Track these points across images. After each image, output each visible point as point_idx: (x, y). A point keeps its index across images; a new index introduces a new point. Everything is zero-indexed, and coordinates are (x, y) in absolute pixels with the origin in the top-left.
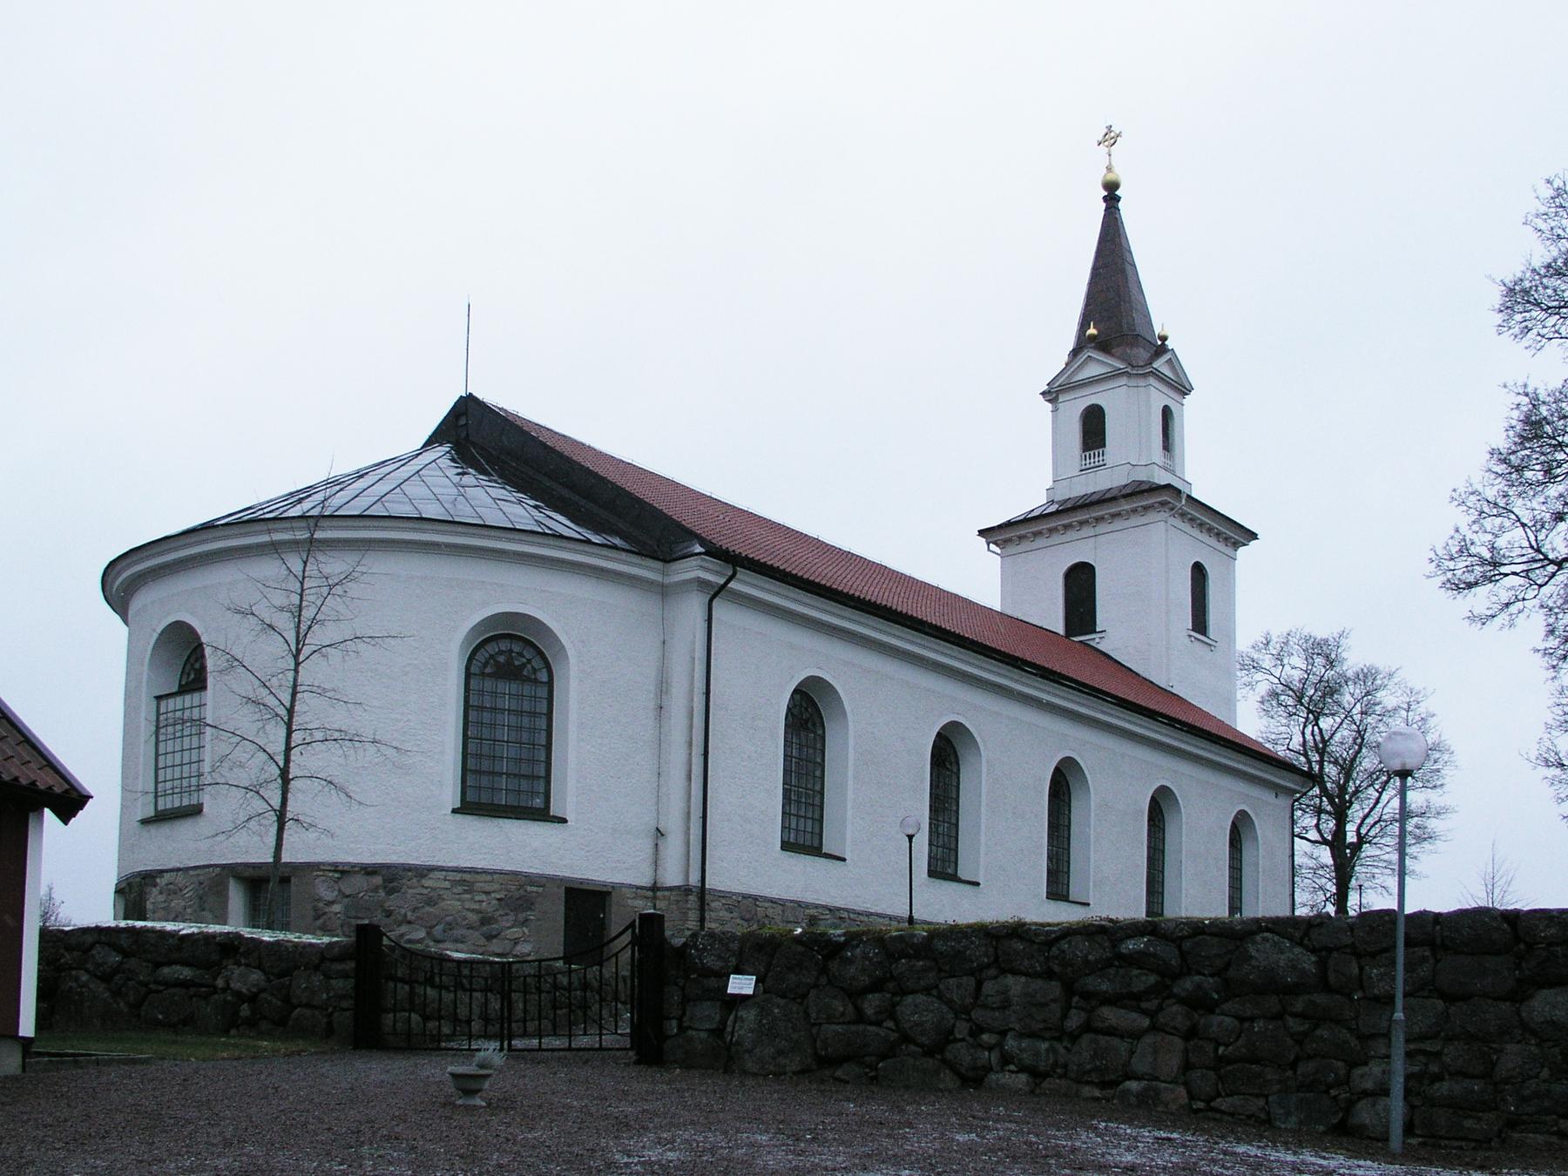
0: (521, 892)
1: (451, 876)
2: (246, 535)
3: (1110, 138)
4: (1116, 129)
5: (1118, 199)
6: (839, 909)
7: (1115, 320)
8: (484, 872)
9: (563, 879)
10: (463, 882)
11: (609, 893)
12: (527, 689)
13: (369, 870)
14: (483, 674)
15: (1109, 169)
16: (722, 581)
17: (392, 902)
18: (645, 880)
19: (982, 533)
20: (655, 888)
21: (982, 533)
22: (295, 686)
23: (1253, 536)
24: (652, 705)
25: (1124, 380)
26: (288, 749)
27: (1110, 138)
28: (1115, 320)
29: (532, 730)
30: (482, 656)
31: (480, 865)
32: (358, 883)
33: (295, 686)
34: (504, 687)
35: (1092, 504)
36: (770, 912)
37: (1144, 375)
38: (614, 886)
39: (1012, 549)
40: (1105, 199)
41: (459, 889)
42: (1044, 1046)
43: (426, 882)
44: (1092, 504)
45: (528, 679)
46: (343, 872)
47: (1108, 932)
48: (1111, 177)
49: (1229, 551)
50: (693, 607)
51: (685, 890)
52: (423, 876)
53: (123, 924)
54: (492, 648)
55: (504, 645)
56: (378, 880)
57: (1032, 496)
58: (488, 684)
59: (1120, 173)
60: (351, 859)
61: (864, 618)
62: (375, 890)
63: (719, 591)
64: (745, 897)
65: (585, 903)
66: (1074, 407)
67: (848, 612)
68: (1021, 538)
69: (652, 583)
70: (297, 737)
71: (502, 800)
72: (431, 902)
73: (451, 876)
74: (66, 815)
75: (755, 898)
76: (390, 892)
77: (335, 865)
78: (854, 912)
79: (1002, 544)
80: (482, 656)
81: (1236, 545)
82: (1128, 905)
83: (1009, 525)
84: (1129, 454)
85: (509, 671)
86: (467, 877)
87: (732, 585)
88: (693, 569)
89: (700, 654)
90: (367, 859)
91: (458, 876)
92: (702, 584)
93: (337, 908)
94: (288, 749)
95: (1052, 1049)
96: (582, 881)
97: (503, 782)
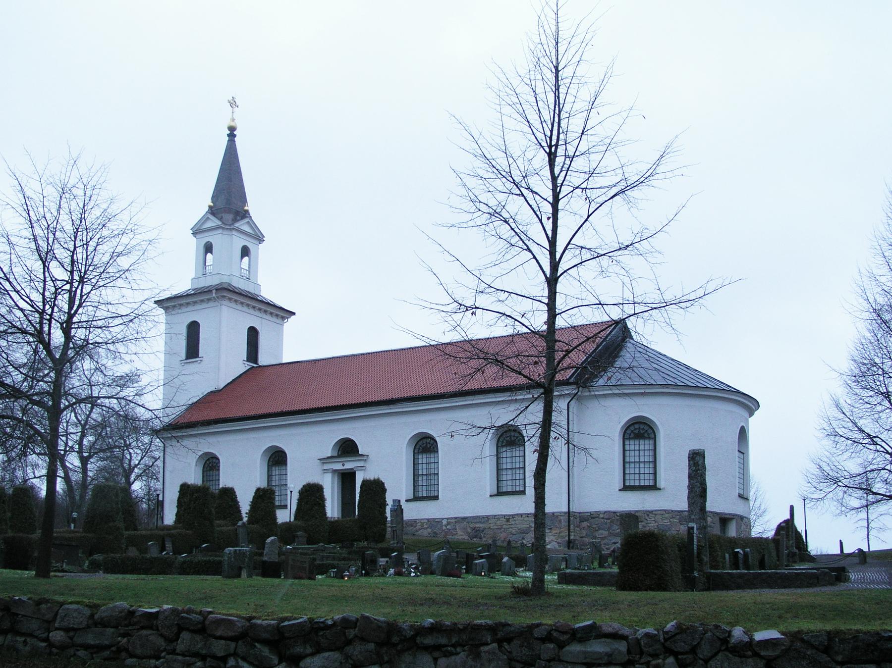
5: (235, 136)
7: (229, 202)
9: (717, 514)
23: (294, 314)
25: (220, 231)
28: (229, 202)
30: (629, 432)
35: (247, 296)
37: (231, 230)
40: (228, 135)
44: (247, 296)
48: (233, 124)
49: (279, 321)
55: (637, 426)
57: (183, 285)
59: (238, 124)
71: (509, 490)
74: (38, 575)
79: (166, 309)
80: (629, 432)
81: (283, 318)
83: (169, 299)
84: (226, 267)
85: (639, 436)
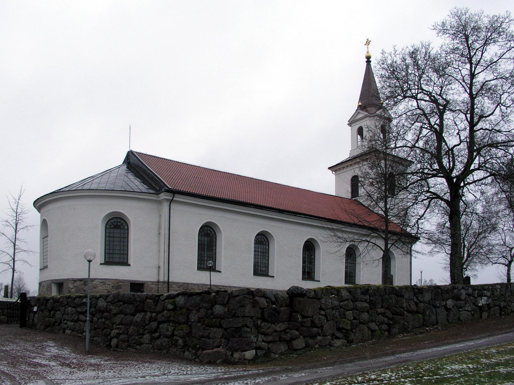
0: (118, 284)
1: (100, 281)
2: (52, 197)
3: (368, 43)
4: (369, 40)
6: (219, 286)
8: (108, 279)
9: (129, 281)
10: (103, 282)
11: (144, 284)
12: (122, 231)
13: (81, 280)
14: (110, 228)
15: (368, 52)
16: (171, 198)
17: (86, 288)
18: (155, 280)
19: (329, 168)
20: (158, 282)
21: (329, 168)
22: (15, 238)
24: (157, 233)
25: (368, 118)
26: (14, 254)
27: (368, 43)
29: (124, 242)
31: (107, 278)
32: (78, 283)
33: (15, 238)
34: (115, 231)
36: (194, 287)
38: (145, 282)
39: (338, 172)
41: (102, 284)
42: (73, 324)
43: (94, 283)
45: (122, 229)
46: (75, 281)
47: (329, 290)
48: (368, 55)
50: (166, 206)
51: (164, 282)
52: (93, 281)
53: (347, 285)
54: (112, 221)
56: (82, 282)
57: (345, 155)
58: (112, 230)
59: (371, 54)
60: (76, 277)
61: (225, 204)
62: (82, 285)
63: (171, 201)
64: (184, 283)
65: (137, 286)
66: (356, 126)
67: (218, 203)
68: (340, 169)
69: (155, 200)
70: (17, 251)
72: (95, 288)
73: (100, 281)
75: (188, 284)
76: (85, 285)
77: (73, 279)
78: (225, 286)
79: (335, 171)
82: (338, 280)
86: (104, 281)
87: (174, 199)
88: (163, 196)
89: (167, 218)
90: (80, 277)
91: (101, 281)
92: (167, 200)
93: (73, 290)
94: (14, 254)
95: (74, 324)
96: (135, 281)
97: (118, 256)
